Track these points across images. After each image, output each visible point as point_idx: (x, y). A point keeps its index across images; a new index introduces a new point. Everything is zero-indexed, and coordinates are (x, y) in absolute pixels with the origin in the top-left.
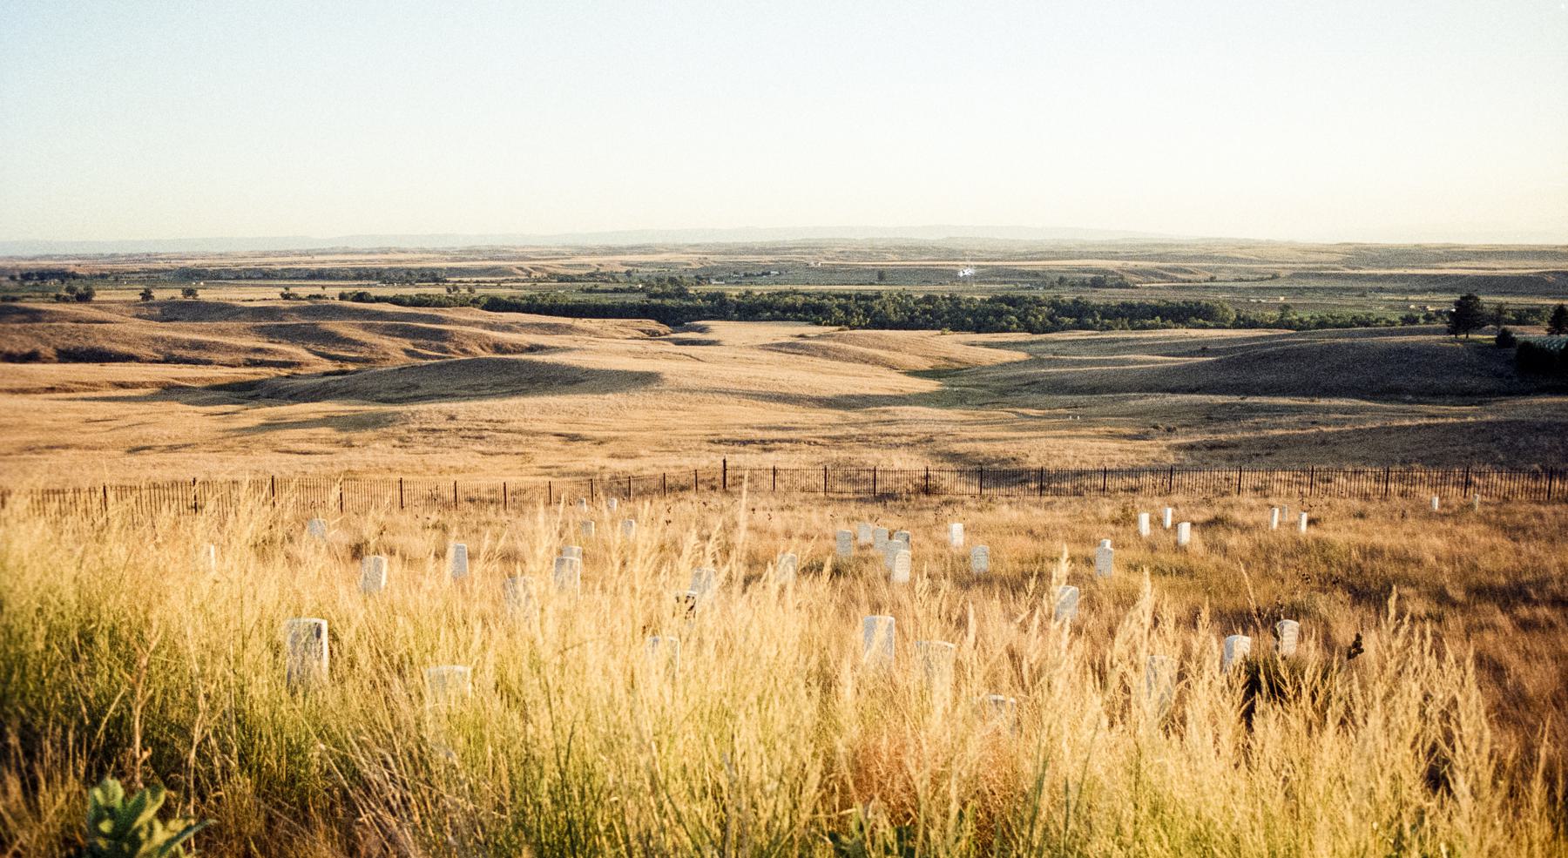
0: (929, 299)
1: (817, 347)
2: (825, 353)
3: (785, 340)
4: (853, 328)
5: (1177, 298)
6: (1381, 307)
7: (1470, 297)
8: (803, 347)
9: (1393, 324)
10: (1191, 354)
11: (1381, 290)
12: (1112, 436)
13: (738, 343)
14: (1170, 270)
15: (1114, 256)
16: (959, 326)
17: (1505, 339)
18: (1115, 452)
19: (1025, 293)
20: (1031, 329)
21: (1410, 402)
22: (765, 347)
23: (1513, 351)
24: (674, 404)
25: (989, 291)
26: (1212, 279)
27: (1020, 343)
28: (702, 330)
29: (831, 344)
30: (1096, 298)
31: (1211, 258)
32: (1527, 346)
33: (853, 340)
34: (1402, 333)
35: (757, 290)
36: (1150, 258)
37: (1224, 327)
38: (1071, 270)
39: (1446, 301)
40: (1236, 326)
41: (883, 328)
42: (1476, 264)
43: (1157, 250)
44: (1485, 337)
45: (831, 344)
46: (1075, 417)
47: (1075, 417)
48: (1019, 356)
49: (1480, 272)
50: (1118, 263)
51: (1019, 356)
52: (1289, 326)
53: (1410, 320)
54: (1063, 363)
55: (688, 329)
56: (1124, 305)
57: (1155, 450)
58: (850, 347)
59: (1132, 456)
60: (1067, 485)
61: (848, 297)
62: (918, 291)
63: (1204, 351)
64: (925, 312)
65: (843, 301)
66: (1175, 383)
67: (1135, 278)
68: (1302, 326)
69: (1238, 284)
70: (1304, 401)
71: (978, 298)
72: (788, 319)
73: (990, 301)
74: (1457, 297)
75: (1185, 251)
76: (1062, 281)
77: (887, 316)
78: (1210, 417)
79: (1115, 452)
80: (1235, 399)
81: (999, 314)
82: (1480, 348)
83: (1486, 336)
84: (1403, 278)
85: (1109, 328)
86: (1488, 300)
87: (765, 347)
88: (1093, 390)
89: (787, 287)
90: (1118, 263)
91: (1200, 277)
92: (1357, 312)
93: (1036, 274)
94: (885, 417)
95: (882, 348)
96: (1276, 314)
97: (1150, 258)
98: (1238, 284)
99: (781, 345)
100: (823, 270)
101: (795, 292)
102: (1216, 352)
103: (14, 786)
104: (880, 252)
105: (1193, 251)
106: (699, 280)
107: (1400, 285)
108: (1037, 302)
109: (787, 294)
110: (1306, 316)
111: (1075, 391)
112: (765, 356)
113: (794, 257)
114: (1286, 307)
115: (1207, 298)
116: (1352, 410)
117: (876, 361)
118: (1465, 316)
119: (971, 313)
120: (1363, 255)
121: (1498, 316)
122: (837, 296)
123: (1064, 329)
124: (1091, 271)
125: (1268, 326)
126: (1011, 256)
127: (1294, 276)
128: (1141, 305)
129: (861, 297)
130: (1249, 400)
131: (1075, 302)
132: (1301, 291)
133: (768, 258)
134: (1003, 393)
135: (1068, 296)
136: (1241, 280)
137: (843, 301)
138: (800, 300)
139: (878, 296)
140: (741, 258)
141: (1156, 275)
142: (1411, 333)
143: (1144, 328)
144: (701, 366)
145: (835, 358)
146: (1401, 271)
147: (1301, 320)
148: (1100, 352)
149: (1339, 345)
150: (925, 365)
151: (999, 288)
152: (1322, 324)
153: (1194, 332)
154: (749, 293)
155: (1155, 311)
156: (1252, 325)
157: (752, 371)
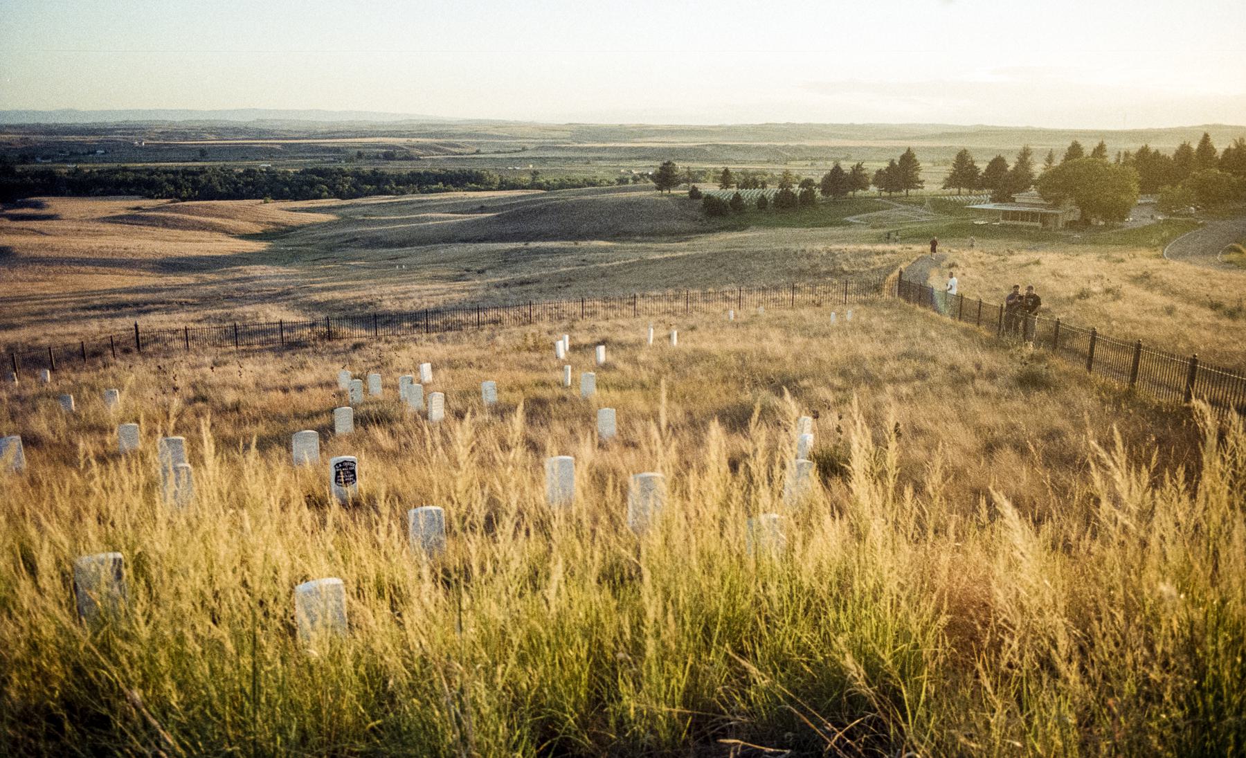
0: (249, 172)
1: (157, 218)
2: (165, 223)
3: (122, 213)
4: (184, 200)
5: (454, 167)
6: (601, 171)
7: (669, 163)
8: (143, 218)
9: (610, 183)
10: (473, 211)
11: (600, 159)
12: (435, 278)
13: (77, 216)
14: (445, 145)
15: (400, 135)
16: (279, 196)
17: (695, 194)
18: (456, 292)
19: (331, 166)
20: (340, 195)
21: (638, 241)
22: (105, 220)
23: (701, 202)
24: (31, 276)
25: (300, 164)
26: (478, 152)
27: (334, 208)
28: (37, 205)
29: (168, 214)
30: (390, 168)
31: (478, 136)
32: (709, 197)
33: (189, 211)
34: (619, 190)
35: (86, 167)
36: (430, 135)
37: (491, 190)
38: (366, 146)
39: (651, 167)
40: (500, 188)
41: (212, 199)
42: (664, 139)
43: (433, 130)
44: (681, 191)
45: (168, 214)
46: (401, 266)
47: (401, 266)
48: (331, 217)
49: (661, 145)
50: (404, 140)
51: (331, 217)
52: (540, 187)
53: (622, 181)
54: (374, 223)
55: (21, 206)
56: (412, 174)
57: (476, 286)
58: (187, 217)
59: (466, 294)
60: (438, 322)
61: (175, 173)
62: (239, 167)
63: (482, 209)
64: (247, 184)
65: (171, 176)
66: (471, 234)
67: (419, 152)
68: (549, 187)
69: (497, 156)
70: (569, 244)
71: (291, 171)
72: (120, 194)
73: (302, 173)
74: (659, 164)
75: (453, 130)
76: (360, 155)
77: (213, 188)
78: (507, 260)
79: (456, 292)
80: (521, 245)
81: (312, 184)
82: (681, 201)
83: (681, 191)
84: (631, 149)
85: (403, 193)
86: (681, 166)
87: (105, 220)
88: (402, 244)
89: (115, 165)
90: (404, 140)
91: (468, 151)
92: (586, 176)
93: (337, 150)
94: (238, 275)
95: (218, 216)
96: (528, 178)
97: (430, 135)
98: (497, 156)
99: (121, 217)
100: (147, 149)
101: (125, 169)
102: (492, 210)
103: (1240, 463)
104: (199, 132)
105: (461, 130)
106: (24, 159)
107: (614, 155)
108: (342, 173)
109: (116, 171)
110: (550, 179)
111: (390, 245)
112: (109, 227)
113: (119, 138)
114: (535, 173)
115: (476, 168)
116: (606, 250)
117: (213, 228)
118: (665, 178)
119: (286, 184)
120: (583, 132)
121: (692, 177)
122: (166, 172)
123: (368, 194)
124: (382, 147)
125: (524, 188)
126: (314, 135)
127: (537, 149)
128: (426, 173)
129: (186, 172)
130: (532, 245)
131: (374, 173)
132: (544, 160)
133: (92, 138)
134: (331, 249)
135: (367, 169)
136: (499, 152)
137: (171, 176)
138: (131, 177)
139: (202, 171)
140: (65, 138)
141: (436, 150)
142: (625, 190)
143: (431, 192)
144: (48, 239)
145: (175, 227)
146: (612, 145)
147: (548, 182)
148: (400, 212)
149: (585, 201)
150: (257, 229)
151: (310, 163)
152: (562, 186)
153: (471, 194)
154: (77, 170)
155: (437, 178)
156: (514, 187)
157: (200, 246)
